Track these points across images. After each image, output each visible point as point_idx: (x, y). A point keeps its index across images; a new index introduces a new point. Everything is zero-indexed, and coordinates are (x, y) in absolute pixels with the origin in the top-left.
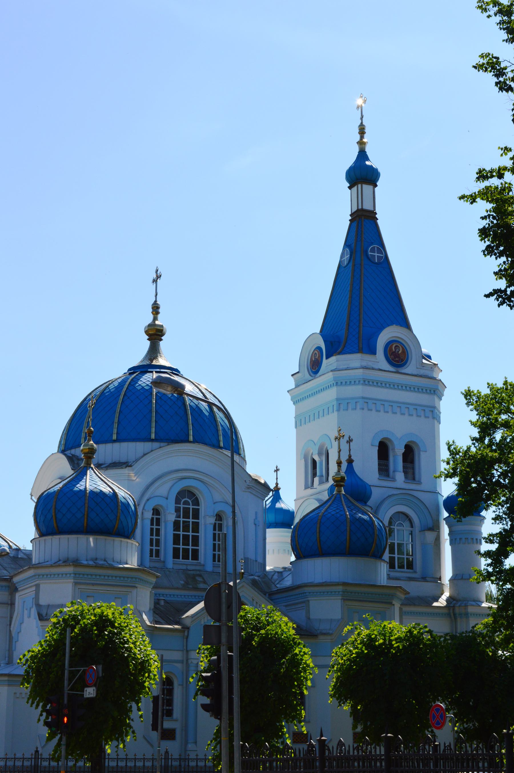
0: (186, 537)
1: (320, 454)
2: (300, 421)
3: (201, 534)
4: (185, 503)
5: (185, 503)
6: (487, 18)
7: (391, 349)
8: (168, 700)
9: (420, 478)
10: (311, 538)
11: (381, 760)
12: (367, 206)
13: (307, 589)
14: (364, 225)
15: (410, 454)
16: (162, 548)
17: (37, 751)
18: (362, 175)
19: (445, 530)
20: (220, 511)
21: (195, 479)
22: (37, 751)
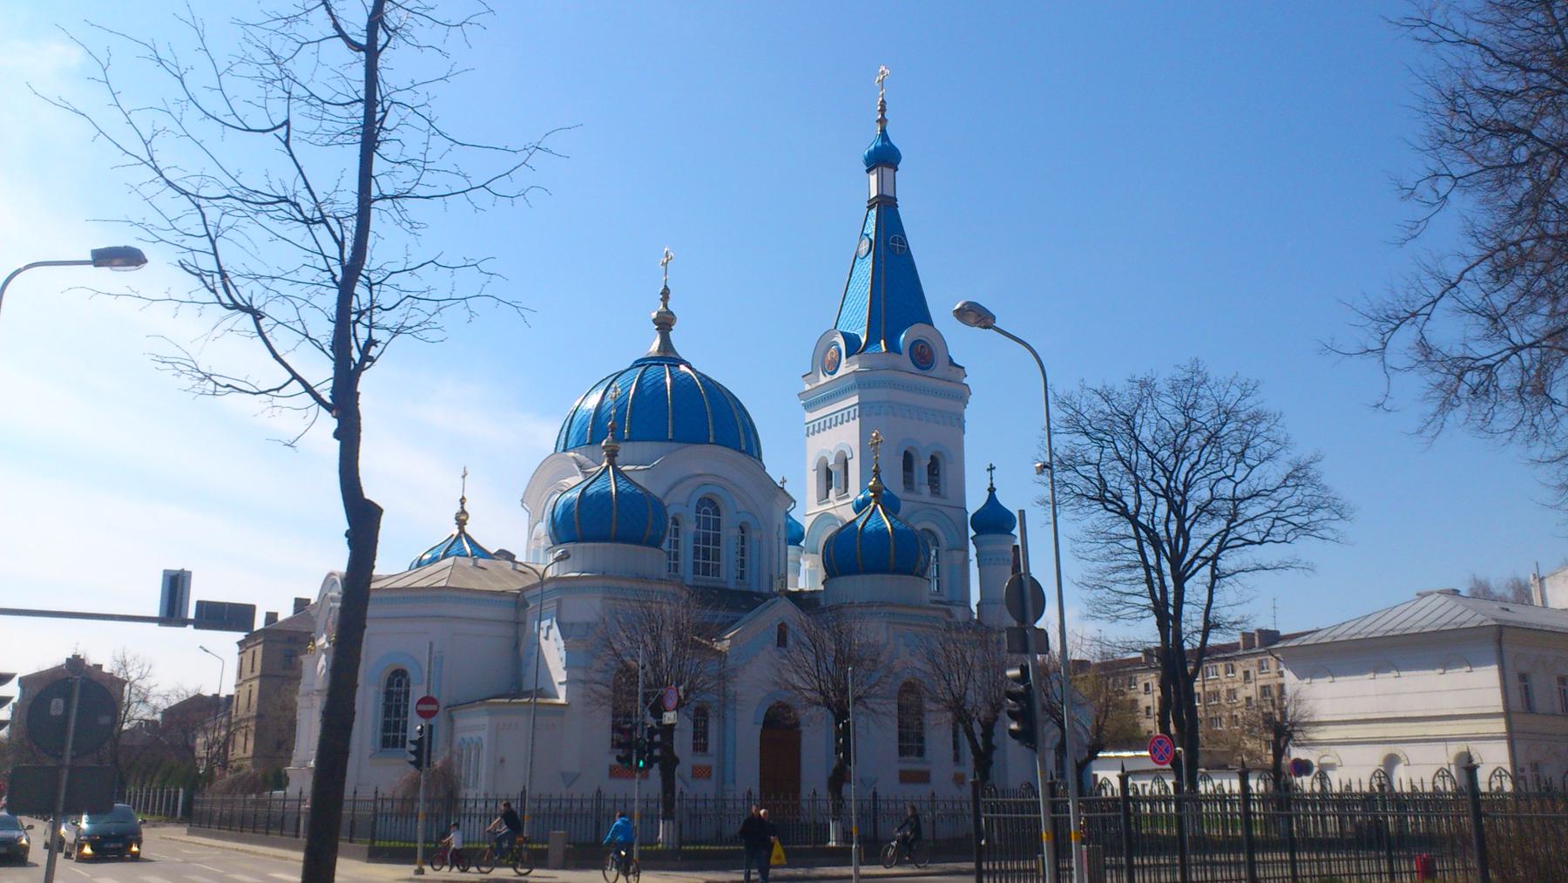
0: (706, 552)
3: (723, 547)
4: (706, 512)
5: (706, 512)
6: (176, 567)
10: (846, 553)
11: (1232, 803)
14: (886, 206)
15: (934, 466)
16: (681, 561)
18: (884, 158)
19: (972, 550)
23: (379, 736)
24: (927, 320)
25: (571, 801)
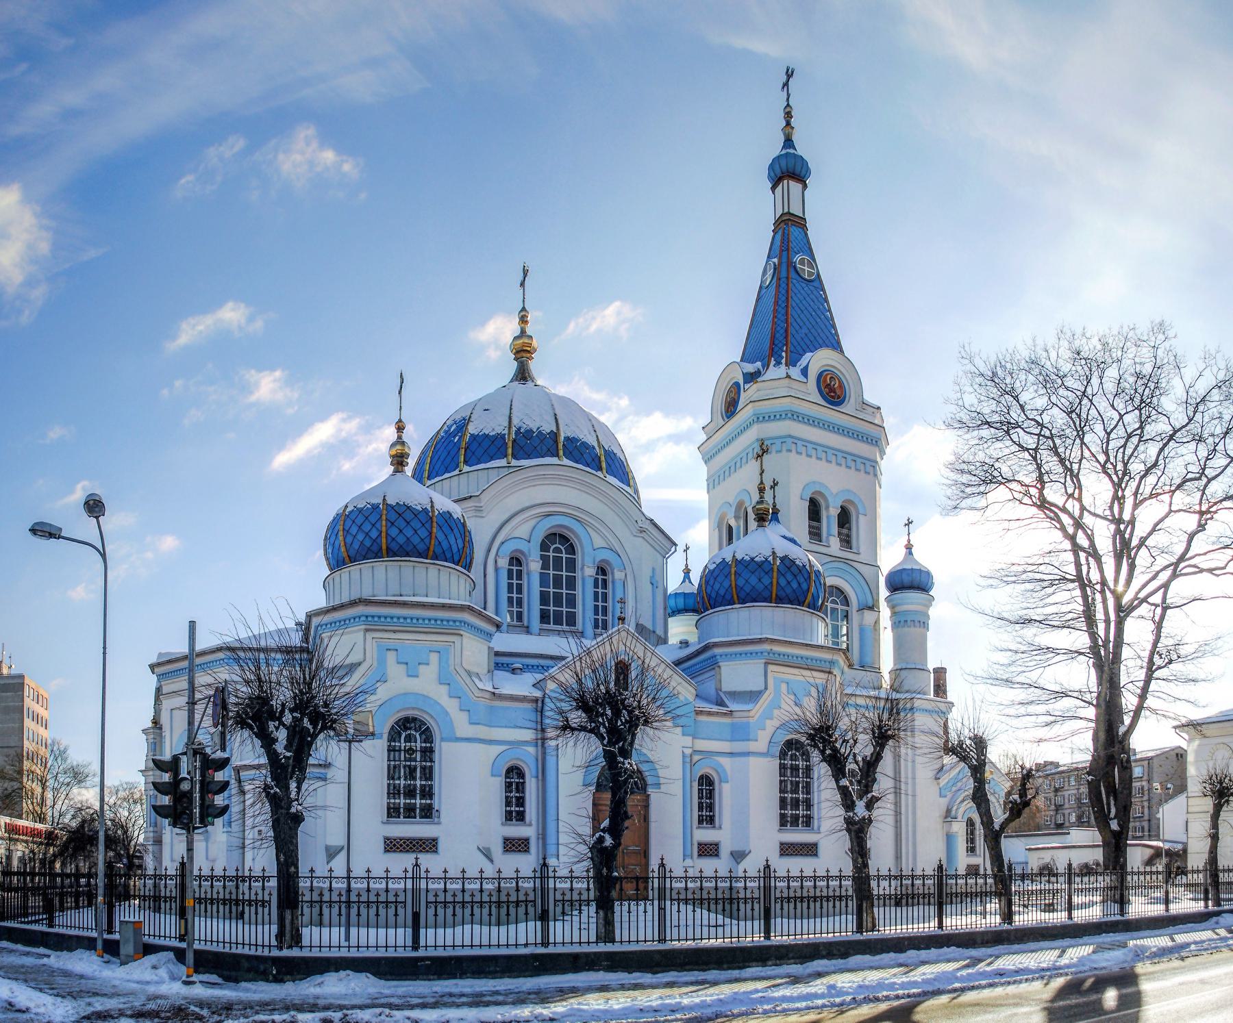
0: (558, 597)
1: (737, 518)
2: (713, 483)
3: (579, 592)
4: (557, 550)
7: (825, 380)
8: (518, 799)
9: (858, 548)
12: (796, 210)
13: (717, 651)
14: (790, 231)
15: (844, 518)
17: (767, 867)
18: (789, 170)
19: (885, 613)
20: (603, 561)
21: (563, 514)
22: (767, 867)
23: (775, 811)
24: (837, 346)
25: (77, 907)
